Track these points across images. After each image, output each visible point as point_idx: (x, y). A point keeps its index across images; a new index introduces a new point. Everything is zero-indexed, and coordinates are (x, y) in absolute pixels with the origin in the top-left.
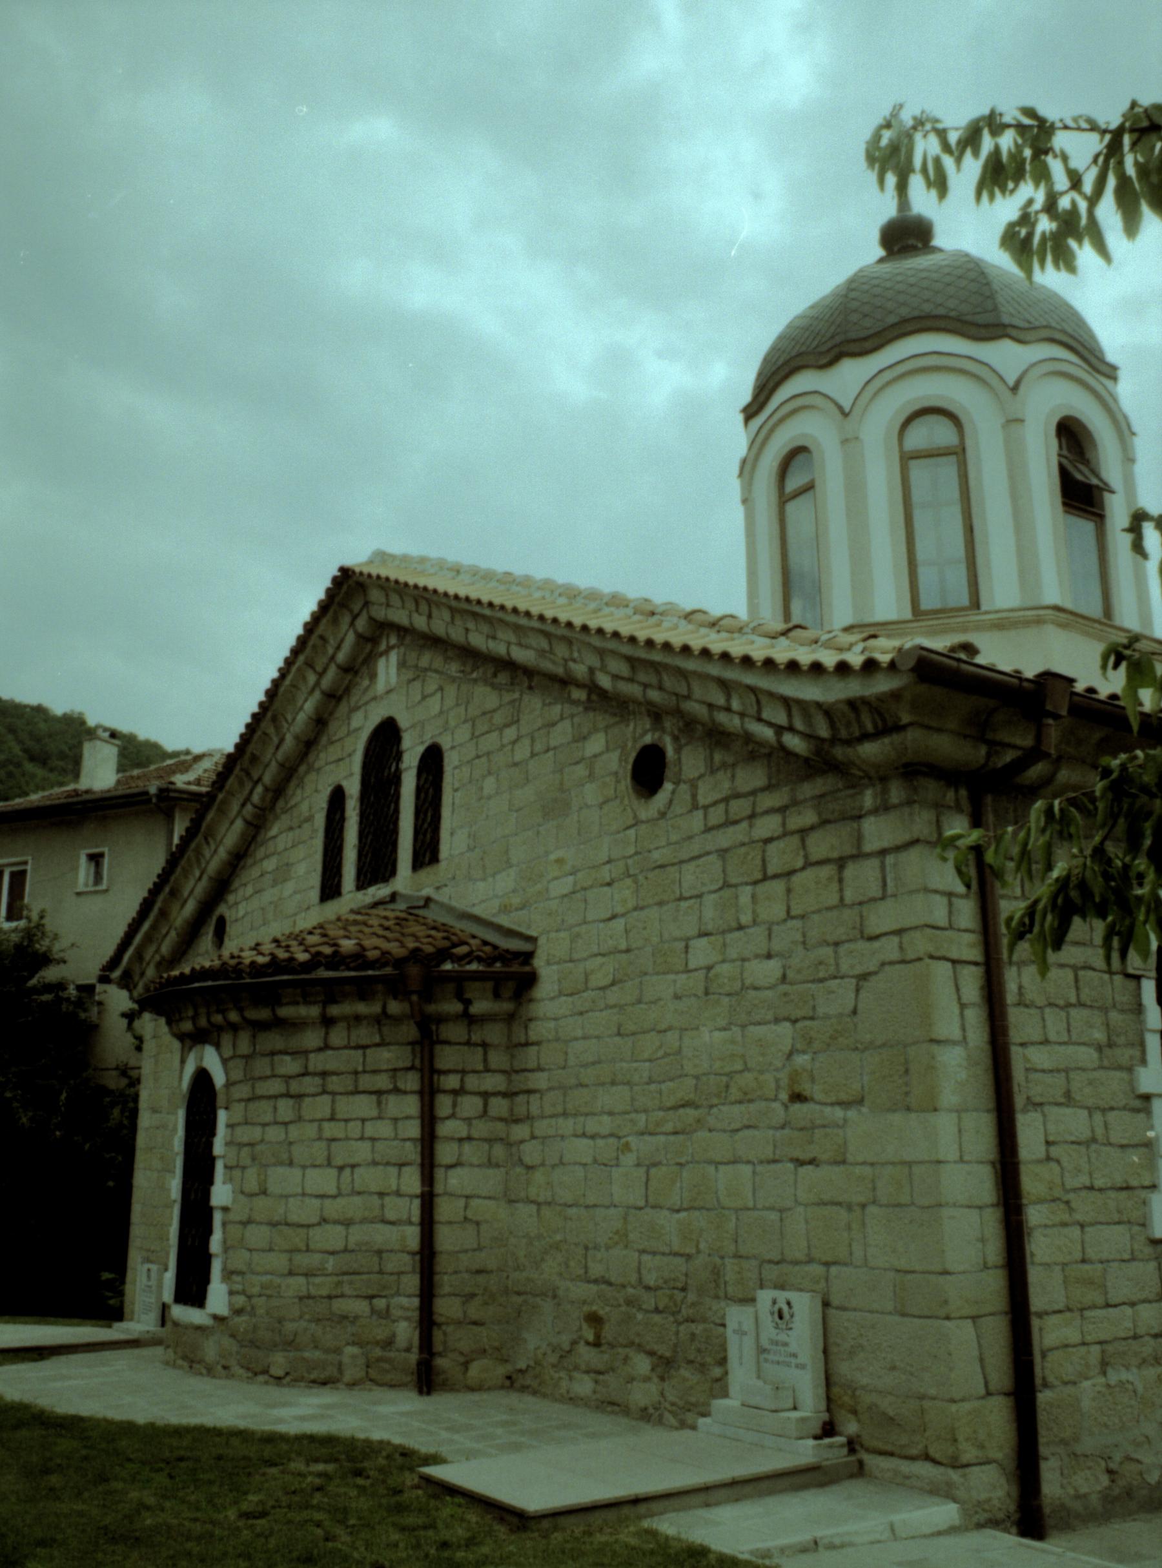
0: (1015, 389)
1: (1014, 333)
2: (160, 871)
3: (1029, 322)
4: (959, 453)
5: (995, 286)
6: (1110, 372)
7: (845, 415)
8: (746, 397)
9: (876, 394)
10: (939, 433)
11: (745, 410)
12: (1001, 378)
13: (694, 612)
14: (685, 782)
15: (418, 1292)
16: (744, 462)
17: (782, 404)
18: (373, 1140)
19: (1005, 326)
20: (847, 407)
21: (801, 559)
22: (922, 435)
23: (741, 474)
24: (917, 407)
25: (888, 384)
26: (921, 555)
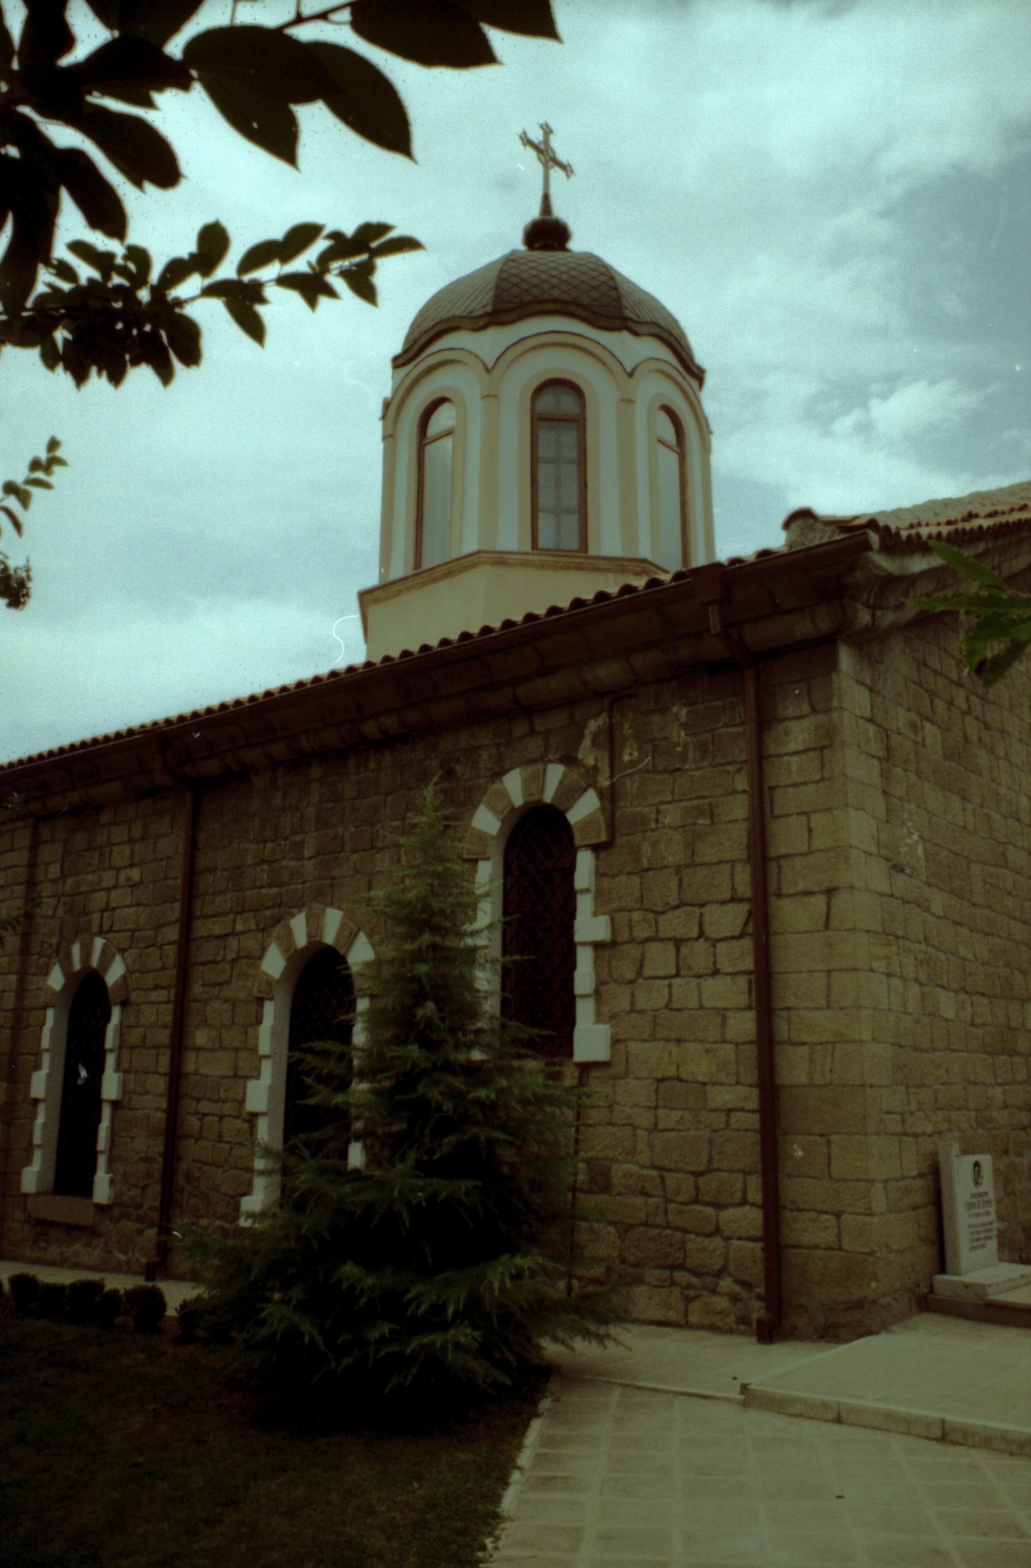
0: (631, 375)
1: (629, 324)
2: (475, 629)
3: (638, 316)
4: (578, 422)
5: (619, 280)
6: (698, 375)
7: (488, 371)
8: (396, 346)
9: (523, 353)
10: (568, 404)
11: (395, 359)
12: (624, 369)
13: (891, 391)
14: (873, 617)
15: (760, 1233)
16: (387, 405)
17: (439, 351)
18: (916, 1136)
19: (627, 319)
20: (490, 366)
21: (669, 460)
22: (548, 402)
23: (384, 417)
24: (538, 382)
25: (534, 348)
26: (543, 502)
